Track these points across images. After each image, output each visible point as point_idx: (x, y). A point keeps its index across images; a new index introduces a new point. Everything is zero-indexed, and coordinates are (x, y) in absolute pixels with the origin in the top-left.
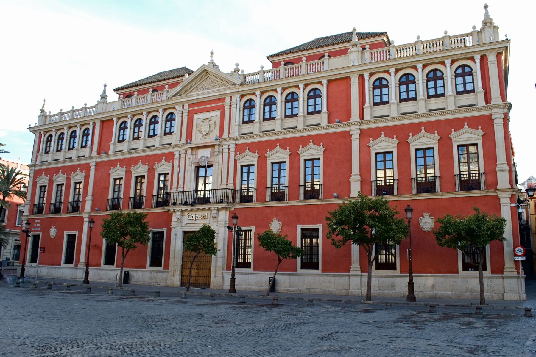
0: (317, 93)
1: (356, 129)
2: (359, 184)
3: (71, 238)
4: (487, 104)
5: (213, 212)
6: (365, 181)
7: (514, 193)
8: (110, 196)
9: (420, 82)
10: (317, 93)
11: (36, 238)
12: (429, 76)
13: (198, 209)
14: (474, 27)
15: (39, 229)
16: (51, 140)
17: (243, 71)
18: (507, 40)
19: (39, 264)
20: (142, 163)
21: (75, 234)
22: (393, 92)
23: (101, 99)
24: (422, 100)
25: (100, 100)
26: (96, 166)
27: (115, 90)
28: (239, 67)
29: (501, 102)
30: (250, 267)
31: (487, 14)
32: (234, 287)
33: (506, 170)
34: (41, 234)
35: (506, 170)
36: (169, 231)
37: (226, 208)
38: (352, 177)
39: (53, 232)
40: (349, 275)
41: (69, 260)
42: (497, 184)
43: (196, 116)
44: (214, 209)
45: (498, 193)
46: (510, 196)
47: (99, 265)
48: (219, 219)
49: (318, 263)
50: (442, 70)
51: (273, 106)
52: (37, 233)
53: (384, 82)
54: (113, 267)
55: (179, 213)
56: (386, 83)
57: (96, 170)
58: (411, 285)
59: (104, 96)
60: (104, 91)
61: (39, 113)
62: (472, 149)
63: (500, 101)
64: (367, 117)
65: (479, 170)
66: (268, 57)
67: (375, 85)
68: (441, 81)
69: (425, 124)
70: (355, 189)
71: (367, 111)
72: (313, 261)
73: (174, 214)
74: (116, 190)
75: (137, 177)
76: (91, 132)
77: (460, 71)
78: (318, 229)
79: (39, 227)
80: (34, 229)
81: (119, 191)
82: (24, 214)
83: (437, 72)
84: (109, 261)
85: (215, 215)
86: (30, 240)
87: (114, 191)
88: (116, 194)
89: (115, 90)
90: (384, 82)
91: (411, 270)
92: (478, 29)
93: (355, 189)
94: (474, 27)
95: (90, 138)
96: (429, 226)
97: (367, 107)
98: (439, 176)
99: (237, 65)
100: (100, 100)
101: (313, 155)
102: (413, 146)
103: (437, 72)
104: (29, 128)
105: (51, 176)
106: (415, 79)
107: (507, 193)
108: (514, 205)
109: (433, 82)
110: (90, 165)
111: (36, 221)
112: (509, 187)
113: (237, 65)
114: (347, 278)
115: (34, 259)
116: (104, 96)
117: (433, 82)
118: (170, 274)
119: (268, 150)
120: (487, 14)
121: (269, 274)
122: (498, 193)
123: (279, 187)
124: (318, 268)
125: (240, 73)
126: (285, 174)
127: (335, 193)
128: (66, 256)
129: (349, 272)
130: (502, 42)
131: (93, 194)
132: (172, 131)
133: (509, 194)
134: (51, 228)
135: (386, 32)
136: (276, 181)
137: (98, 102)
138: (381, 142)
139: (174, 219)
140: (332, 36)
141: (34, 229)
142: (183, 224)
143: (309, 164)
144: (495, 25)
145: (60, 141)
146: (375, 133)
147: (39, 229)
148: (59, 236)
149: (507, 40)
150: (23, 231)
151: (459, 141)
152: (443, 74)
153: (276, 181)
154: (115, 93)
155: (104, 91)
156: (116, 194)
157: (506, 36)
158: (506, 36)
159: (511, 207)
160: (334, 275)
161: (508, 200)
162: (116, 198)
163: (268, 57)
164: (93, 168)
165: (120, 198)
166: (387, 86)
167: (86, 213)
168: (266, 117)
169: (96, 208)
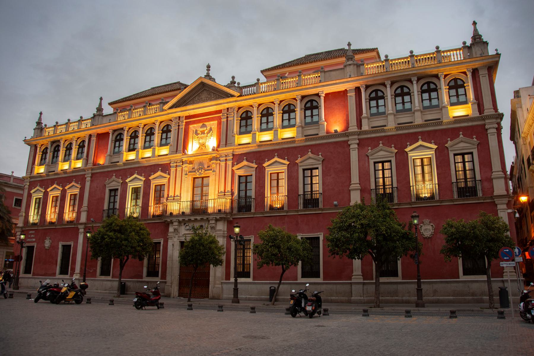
0: (249, 115)
1: (354, 139)
2: (358, 192)
3: (66, 249)
4: (480, 114)
5: (211, 222)
6: (364, 190)
7: (510, 199)
8: (106, 207)
9: (416, 93)
10: (249, 115)
11: (30, 249)
12: (397, 92)
13: (196, 219)
14: (464, 43)
15: (34, 240)
16: (59, 150)
17: (239, 84)
18: (497, 54)
19: (34, 274)
20: (116, 176)
21: (71, 245)
22: (277, 118)
23: (97, 112)
24: (418, 110)
25: (96, 113)
26: (91, 177)
27: (110, 104)
28: (235, 80)
29: (494, 113)
30: (158, 276)
31: (475, 30)
32: (237, 297)
33: (501, 178)
34: (35, 245)
35: (501, 178)
36: (166, 242)
37: (224, 218)
38: (493, 174)
39: (47, 243)
40: (351, 283)
41: (64, 271)
42: (494, 192)
43: (191, 126)
44: (212, 220)
45: (495, 200)
46: (506, 202)
47: (54, 274)
48: (217, 229)
49: (249, 273)
50: (435, 82)
51: (249, 121)
52: (31, 244)
53: (380, 94)
54: (110, 278)
55: (176, 224)
56: (382, 94)
57: (92, 181)
58: (419, 290)
59: (100, 109)
60: (100, 104)
61: (35, 126)
62: (387, 165)
63: (492, 112)
64: (365, 127)
65: (392, 185)
66: (262, 72)
67: (371, 96)
68: (383, 100)
69: (422, 133)
70: (355, 198)
71: (365, 122)
72: (239, 271)
73: (170, 225)
74: (112, 200)
75: (111, 191)
76: (86, 145)
77: (399, 91)
78: (319, 238)
79: (33, 238)
80: (29, 240)
81: (114, 202)
82: (18, 225)
83: (379, 92)
84: (105, 272)
85: (214, 225)
86: (24, 251)
87: (109, 202)
88: (112, 205)
89: (110, 104)
90: (380, 94)
91: (419, 276)
92: (468, 44)
93: (355, 198)
94: (464, 43)
95: (86, 149)
96: (430, 233)
97: (365, 118)
98: (397, 188)
99: (233, 78)
100: (96, 113)
101: (312, 165)
102: (300, 166)
103: (379, 92)
104: (25, 141)
105: (147, 176)
106: (410, 90)
107: (504, 199)
108: (510, 211)
109: (287, 115)
110: (86, 176)
111: (31, 232)
112: (505, 193)
113: (233, 78)
114: (349, 286)
115: (27, 271)
116: (100, 109)
117: (287, 115)
118: (167, 284)
119: (266, 160)
120: (475, 30)
121: (270, 283)
122: (495, 200)
123: (312, 194)
124: (249, 277)
125: (236, 85)
126: (252, 186)
127: (335, 201)
128: (61, 268)
129: (351, 279)
130: (493, 56)
131: (88, 205)
132: (168, 142)
133: (506, 200)
134: (46, 239)
135: (377, 48)
136: (308, 188)
137: (94, 114)
138: (112, 182)
139: (171, 229)
140: (322, 53)
141: (29, 240)
142: (181, 235)
143: (308, 173)
144: (484, 40)
145: (56, 153)
146: (373, 142)
147: (34, 240)
148: (54, 247)
149: (497, 54)
150: (18, 242)
151: (455, 150)
152: (437, 86)
153: (308, 188)
154: (110, 107)
155: (100, 104)
156: (112, 205)
157: (496, 50)
158: (496, 50)
159: (508, 213)
160: (262, 283)
161: (505, 206)
162: (111, 209)
163: (262, 72)
164: (88, 179)
165: (116, 209)
166: (383, 98)
167: (81, 224)
168: (242, 131)
169: (92, 219)
